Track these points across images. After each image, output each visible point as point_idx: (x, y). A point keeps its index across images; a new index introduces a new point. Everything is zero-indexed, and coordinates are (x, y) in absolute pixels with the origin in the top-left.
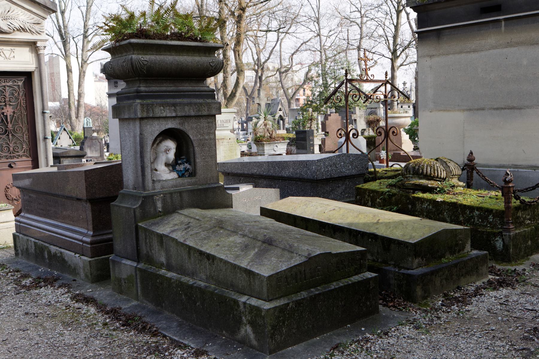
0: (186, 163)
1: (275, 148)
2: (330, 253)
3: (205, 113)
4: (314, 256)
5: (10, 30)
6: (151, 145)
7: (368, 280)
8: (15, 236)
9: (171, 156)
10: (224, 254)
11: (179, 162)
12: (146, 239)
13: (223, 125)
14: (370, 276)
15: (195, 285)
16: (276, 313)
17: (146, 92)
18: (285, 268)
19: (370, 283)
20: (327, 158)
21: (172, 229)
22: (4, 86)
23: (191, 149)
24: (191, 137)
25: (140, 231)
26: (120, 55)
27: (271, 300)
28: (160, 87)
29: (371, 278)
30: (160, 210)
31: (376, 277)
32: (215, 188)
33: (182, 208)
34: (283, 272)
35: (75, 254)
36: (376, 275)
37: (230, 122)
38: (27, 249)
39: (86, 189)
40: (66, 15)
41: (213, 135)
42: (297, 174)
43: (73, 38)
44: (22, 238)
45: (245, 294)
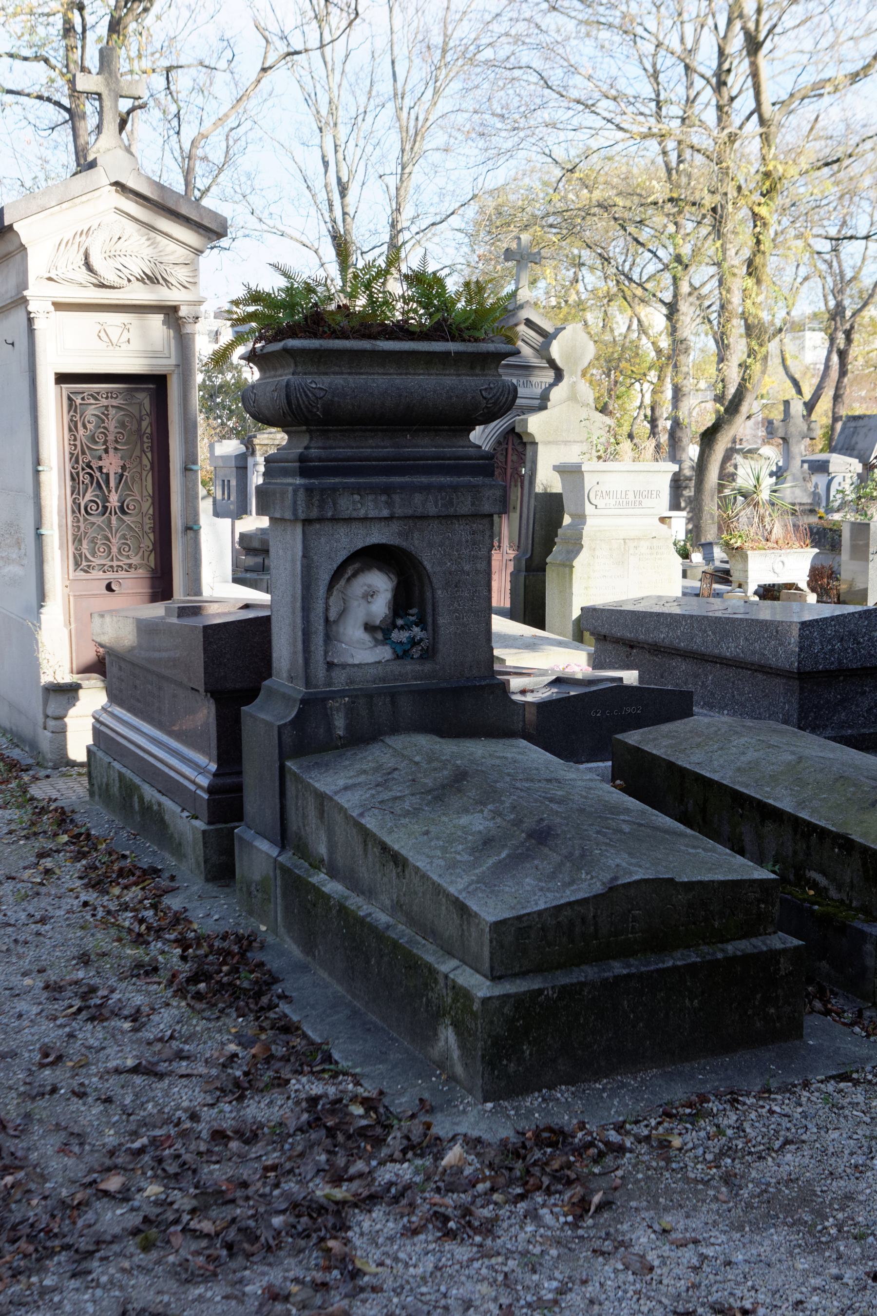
0: (417, 626)
1: (778, 567)
2: (672, 880)
3: (465, 508)
4: (624, 885)
5: (120, 281)
6: (327, 582)
7: (774, 955)
8: (89, 751)
9: (380, 607)
10: (428, 856)
11: (400, 622)
12: (297, 796)
13: (640, 503)
14: (779, 946)
15: (368, 919)
16: (506, 1010)
17: (320, 460)
18: (542, 906)
19: (778, 962)
20: (832, 618)
21: (350, 782)
22: (107, 407)
23: (429, 594)
24: (428, 567)
25: (288, 777)
26: (273, 373)
27: (500, 978)
28: (357, 447)
29: (784, 951)
30: (341, 733)
31: (797, 948)
32: (482, 687)
33: (395, 730)
34: (535, 916)
35: (182, 811)
36: (801, 942)
37: (658, 495)
38: (107, 785)
39: (206, 668)
40: (351, 198)
41: (485, 563)
42: (753, 652)
43: (362, 253)
44: (101, 759)
45: (454, 956)
